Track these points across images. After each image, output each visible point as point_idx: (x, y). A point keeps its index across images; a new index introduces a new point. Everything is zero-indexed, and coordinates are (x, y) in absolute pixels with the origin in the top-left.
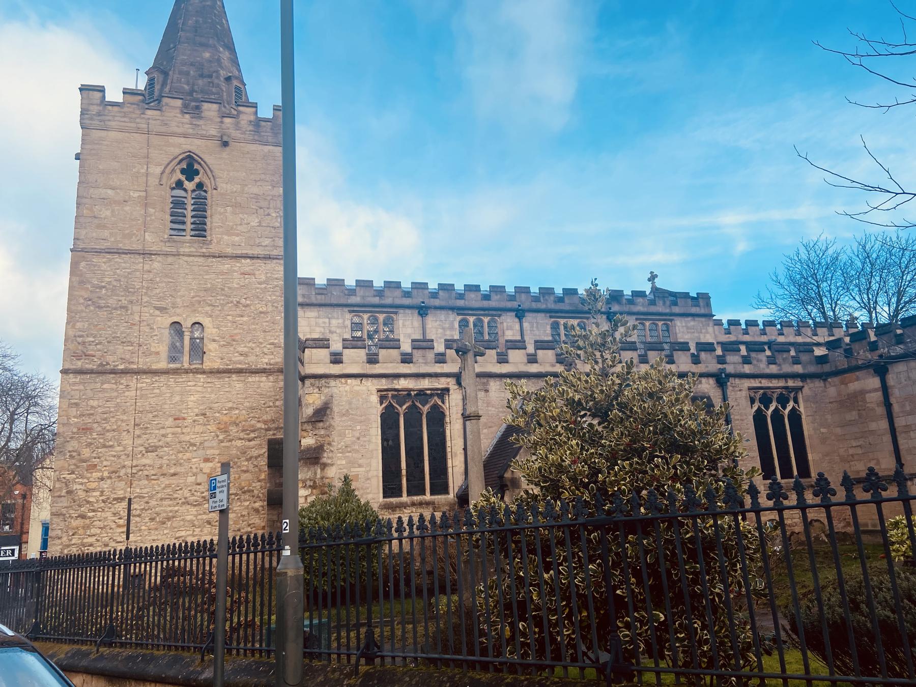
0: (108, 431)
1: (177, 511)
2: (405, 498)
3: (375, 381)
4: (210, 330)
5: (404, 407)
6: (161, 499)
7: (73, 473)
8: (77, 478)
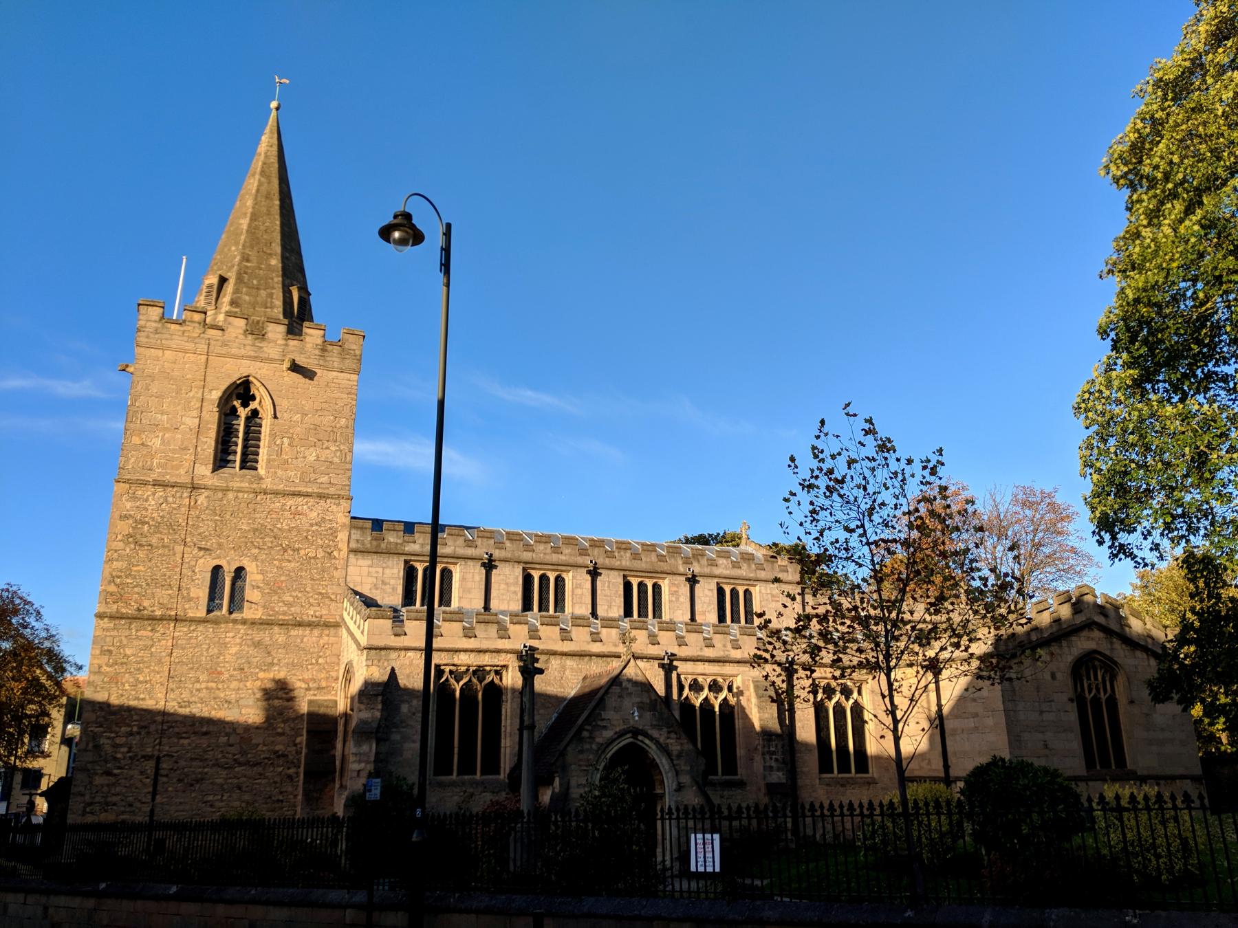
0: (141, 682)
1: (206, 773)
4: (253, 575)
5: (461, 683)
6: (192, 759)
7: (101, 726)
8: (105, 732)
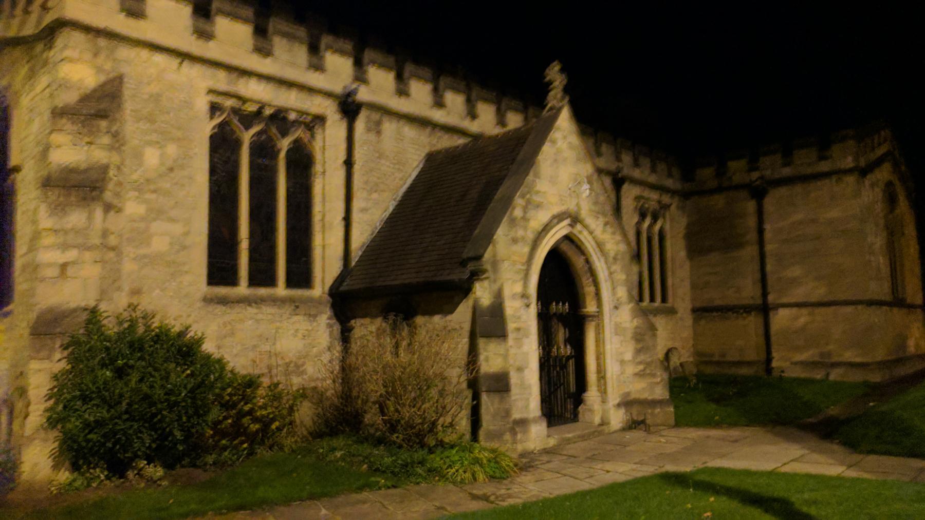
2: (243, 289)
3: (209, 71)
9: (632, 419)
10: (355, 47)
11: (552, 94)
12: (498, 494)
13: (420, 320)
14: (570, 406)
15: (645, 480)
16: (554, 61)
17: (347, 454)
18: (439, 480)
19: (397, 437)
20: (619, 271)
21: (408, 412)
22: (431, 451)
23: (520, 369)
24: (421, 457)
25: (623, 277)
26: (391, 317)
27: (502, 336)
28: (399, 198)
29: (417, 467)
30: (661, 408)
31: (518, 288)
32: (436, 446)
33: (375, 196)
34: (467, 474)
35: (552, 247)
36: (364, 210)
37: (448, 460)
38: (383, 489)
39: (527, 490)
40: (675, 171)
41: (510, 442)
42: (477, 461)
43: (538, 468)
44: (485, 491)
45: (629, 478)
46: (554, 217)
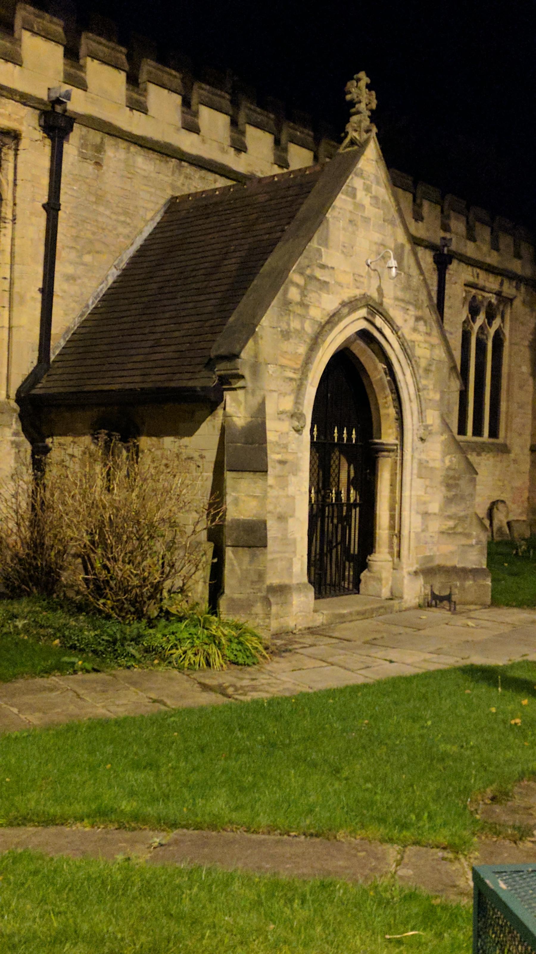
9: (433, 593)
10: (66, 30)
11: (355, 119)
12: (238, 685)
13: (145, 442)
14: (349, 573)
15: (442, 673)
16: (362, 70)
17: (33, 624)
18: (159, 664)
19: (104, 604)
20: (431, 387)
21: (121, 570)
22: (151, 624)
23: (282, 518)
24: (135, 631)
25: (437, 397)
26: (103, 436)
27: (263, 471)
28: (123, 265)
29: (129, 645)
30: (475, 581)
31: (287, 404)
32: (158, 617)
33: (88, 258)
34: (198, 657)
35: (339, 347)
36: (71, 278)
37: (172, 638)
38: (80, 673)
39: (278, 681)
40: (526, 250)
41: (261, 616)
42: (213, 639)
43: (297, 653)
44: (221, 681)
45: (420, 671)
46: (344, 304)
